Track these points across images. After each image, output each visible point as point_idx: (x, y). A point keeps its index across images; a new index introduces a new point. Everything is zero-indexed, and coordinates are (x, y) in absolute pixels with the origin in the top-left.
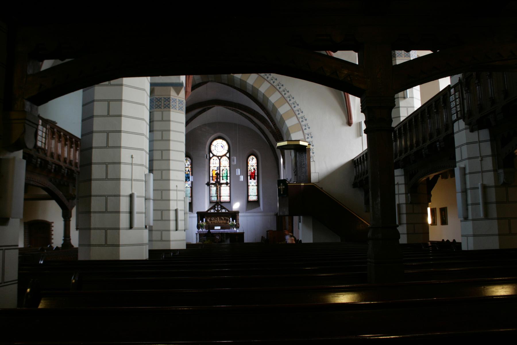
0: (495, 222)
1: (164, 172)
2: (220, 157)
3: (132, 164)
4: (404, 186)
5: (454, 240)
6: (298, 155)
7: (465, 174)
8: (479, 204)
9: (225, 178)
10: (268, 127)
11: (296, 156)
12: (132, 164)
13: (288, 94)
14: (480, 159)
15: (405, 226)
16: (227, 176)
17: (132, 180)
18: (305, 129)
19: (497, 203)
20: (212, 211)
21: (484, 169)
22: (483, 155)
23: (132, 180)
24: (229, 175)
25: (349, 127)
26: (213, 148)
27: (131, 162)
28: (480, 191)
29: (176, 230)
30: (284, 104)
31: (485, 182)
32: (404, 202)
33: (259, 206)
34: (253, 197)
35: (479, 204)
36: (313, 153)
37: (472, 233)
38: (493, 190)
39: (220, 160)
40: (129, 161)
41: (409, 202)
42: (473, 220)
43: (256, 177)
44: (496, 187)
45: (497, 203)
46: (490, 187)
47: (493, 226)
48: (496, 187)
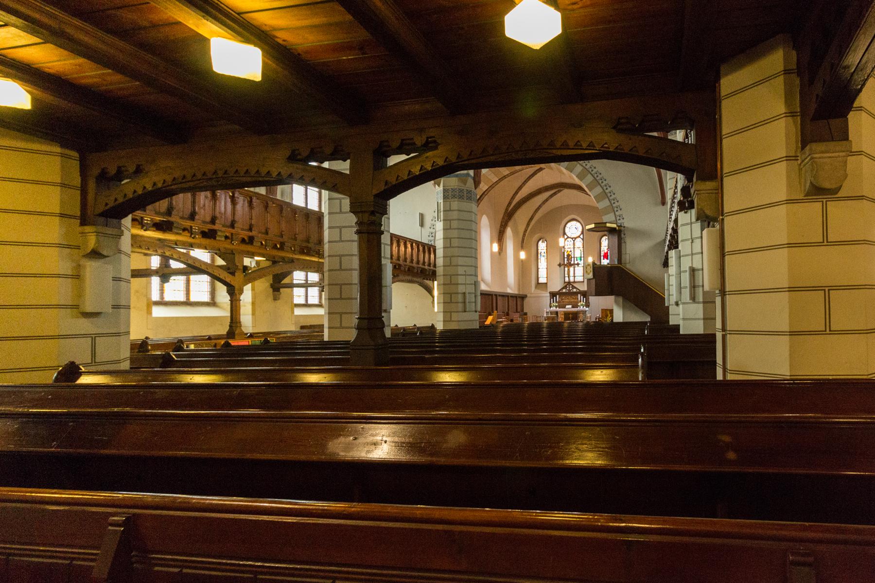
0: (701, 305)
2: (574, 239)
20: (564, 291)
26: (567, 230)
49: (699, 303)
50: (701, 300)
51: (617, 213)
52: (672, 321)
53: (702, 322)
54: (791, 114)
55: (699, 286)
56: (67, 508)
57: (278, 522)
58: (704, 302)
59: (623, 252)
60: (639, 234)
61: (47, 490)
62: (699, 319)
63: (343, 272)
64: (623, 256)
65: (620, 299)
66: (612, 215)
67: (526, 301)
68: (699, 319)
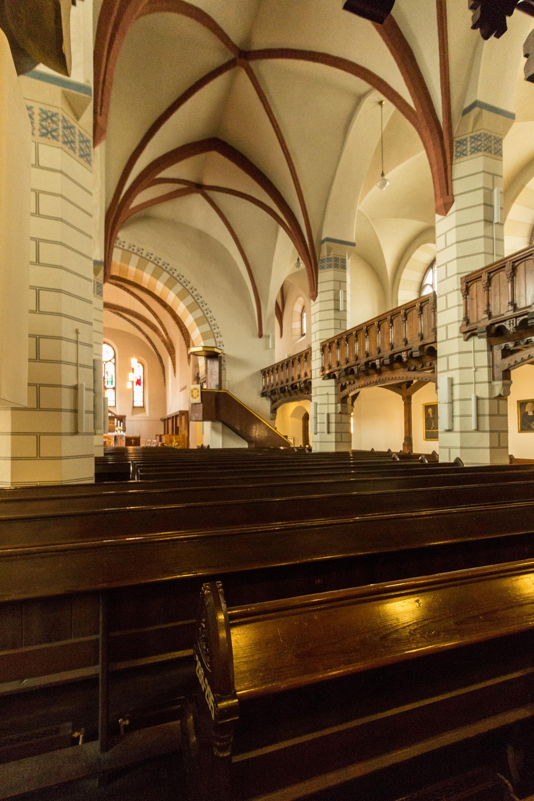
0: (488, 435)
1: (342, 321)
3: (77, 342)
4: (334, 396)
5: (208, 446)
6: (209, 361)
7: (452, 385)
8: (471, 416)
9: (110, 383)
10: (160, 335)
11: (206, 363)
12: (77, 342)
13: (200, 300)
14: (473, 369)
15: (334, 434)
16: (112, 382)
17: (77, 365)
18: (217, 337)
19: (490, 415)
21: (478, 380)
22: (477, 365)
23: (77, 365)
24: (114, 380)
25: (258, 340)
27: (76, 339)
28: (473, 403)
29: (76, 433)
30: (196, 309)
31: (479, 395)
32: (334, 412)
33: (145, 411)
34: (138, 403)
35: (471, 416)
36: (224, 361)
37: (459, 445)
38: (487, 402)
39: (106, 362)
40: (73, 337)
41: (338, 412)
42: (461, 432)
43: (142, 384)
44: (490, 399)
45: (490, 415)
46: (483, 399)
47: (332, 437)
48: (490, 399)
49: (484, 431)
50: (487, 428)
51: (217, 340)
52: (84, 473)
53: (488, 451)
54: (462, 290)
55: (484, 415)
56: (142, 662)
57: (404, 705)
58: (491, 431)
59: (223, 378)
60: (239, 362)
61: (396, 581)
62: (486, 448)
63: (450, 310)
64: (223, 382)
65: (219, 425)
66: (213, 340)
67: (309, 401)
68: (486, 448)
